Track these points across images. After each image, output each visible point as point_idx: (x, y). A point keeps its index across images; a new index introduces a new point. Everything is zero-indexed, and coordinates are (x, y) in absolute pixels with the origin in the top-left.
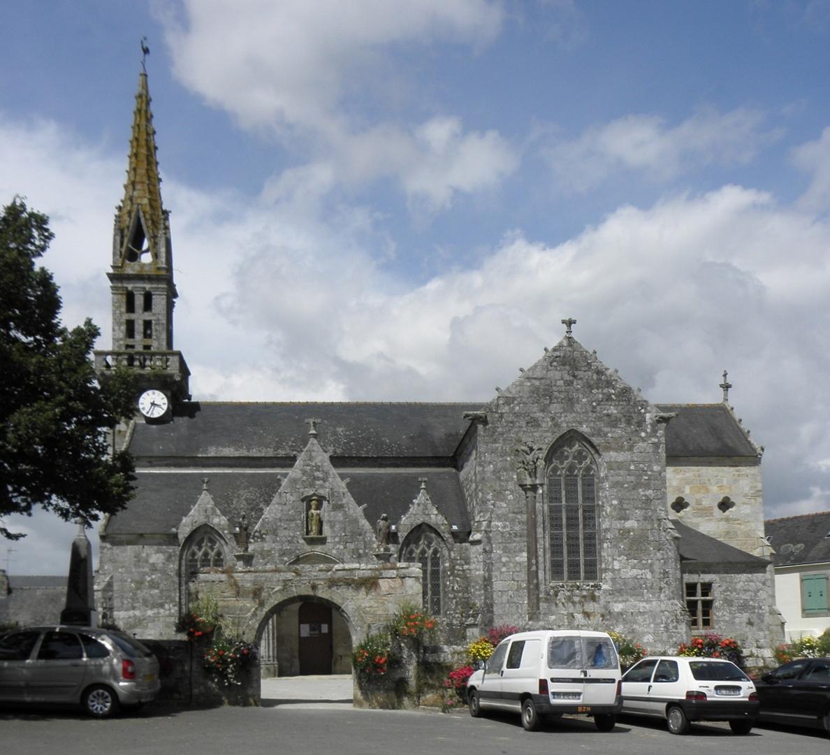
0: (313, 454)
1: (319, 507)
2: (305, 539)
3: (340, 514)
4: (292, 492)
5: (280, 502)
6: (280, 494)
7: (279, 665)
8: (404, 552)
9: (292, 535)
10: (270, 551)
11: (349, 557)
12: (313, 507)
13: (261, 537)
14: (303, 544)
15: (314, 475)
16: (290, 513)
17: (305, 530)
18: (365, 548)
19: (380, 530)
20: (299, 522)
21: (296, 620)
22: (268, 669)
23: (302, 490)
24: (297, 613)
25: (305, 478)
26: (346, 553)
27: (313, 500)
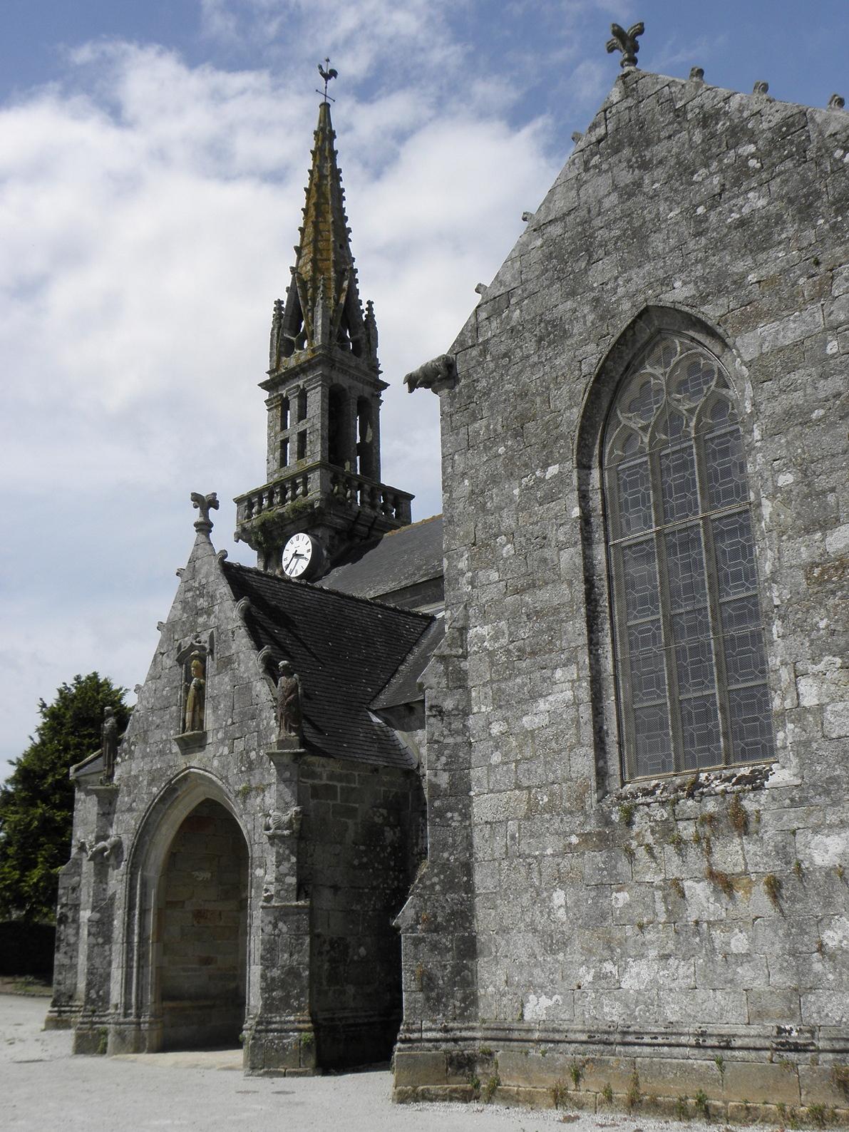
22: (121, 1035)
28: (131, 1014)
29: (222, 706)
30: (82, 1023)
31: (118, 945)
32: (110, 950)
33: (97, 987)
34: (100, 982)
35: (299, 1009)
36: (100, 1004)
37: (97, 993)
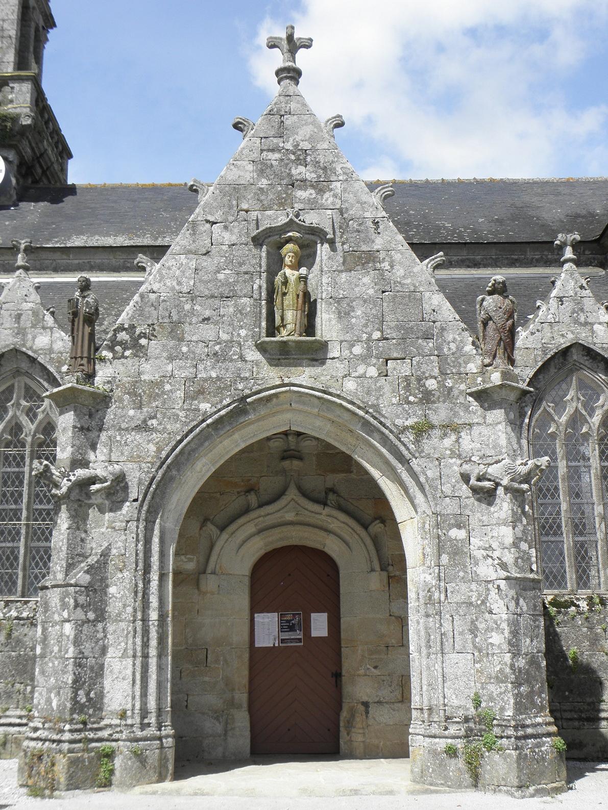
0: (289, 121)
1: (306, 258)
2: (262, 348)
3: (366, 280)
4: (226, 220)
5: (193, 247)
6: (194, 224)
7: (178, 738)
8: (527, 420)
9: (224, 337)
10: (159, 384)
11: (395, 401)
12: (287, 260)
13: (135, 345)
14: (257, 363)
15: (290, 175)
16: (221, 276)
17: (264, 324)
18: (443, 373)
19: (485, 324)
20: (245, 300)
21: (243, 600)
22: (140, 757)
23: (253, 215)
24: (247, 581)
25: (264, 183)
26: (387, 389)
27: (289, 240)
28: (149, 725)
29: (359, 313)
30: (71, 742)
31: (123, 625)
32: (104, 630)
33: (86, 686)
34: (91, 678)
35: (542, 709)
36: (91, 711)
37: (88, 694)
